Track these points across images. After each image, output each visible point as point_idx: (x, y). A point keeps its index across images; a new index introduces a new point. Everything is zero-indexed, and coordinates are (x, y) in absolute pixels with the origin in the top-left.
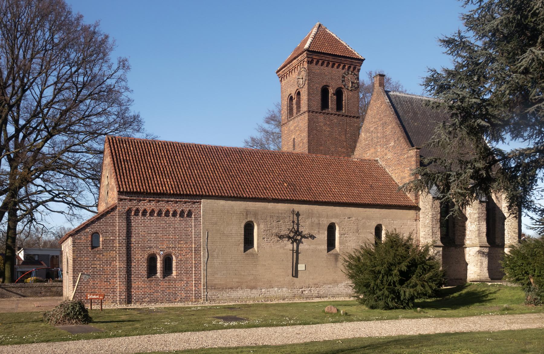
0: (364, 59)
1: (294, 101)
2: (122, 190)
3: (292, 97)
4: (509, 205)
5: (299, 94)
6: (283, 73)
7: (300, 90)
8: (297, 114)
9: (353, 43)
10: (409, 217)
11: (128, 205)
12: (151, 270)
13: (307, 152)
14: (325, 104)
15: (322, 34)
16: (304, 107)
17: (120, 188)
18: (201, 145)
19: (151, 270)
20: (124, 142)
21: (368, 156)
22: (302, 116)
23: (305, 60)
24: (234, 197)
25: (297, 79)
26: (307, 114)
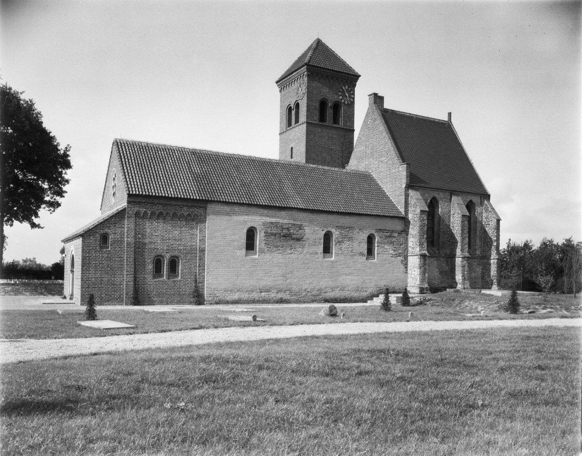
0: (360, 76)
1: (293, 112)
2: (131, 193)
3: (291, 107)
4: (559, 246)
5: (297, 106)
6: (283, 82)
7: (299, 102)
8: (295, 124)
9: (350, 54)
10: (472, 371)
11: (136, 209)
12: (158, 270)
13: (304, 161)
14: (322, 118)
15: (319, 47)
16: (303, 118)
17: (129, 191)
18: (184, 148)
19: (158, 270)
20: (164, 150)
21: (361, 168)
22: (300, 127)
23: (306, 73)
24: (232, 203)
25: (299, 91)
26: (305, 125)
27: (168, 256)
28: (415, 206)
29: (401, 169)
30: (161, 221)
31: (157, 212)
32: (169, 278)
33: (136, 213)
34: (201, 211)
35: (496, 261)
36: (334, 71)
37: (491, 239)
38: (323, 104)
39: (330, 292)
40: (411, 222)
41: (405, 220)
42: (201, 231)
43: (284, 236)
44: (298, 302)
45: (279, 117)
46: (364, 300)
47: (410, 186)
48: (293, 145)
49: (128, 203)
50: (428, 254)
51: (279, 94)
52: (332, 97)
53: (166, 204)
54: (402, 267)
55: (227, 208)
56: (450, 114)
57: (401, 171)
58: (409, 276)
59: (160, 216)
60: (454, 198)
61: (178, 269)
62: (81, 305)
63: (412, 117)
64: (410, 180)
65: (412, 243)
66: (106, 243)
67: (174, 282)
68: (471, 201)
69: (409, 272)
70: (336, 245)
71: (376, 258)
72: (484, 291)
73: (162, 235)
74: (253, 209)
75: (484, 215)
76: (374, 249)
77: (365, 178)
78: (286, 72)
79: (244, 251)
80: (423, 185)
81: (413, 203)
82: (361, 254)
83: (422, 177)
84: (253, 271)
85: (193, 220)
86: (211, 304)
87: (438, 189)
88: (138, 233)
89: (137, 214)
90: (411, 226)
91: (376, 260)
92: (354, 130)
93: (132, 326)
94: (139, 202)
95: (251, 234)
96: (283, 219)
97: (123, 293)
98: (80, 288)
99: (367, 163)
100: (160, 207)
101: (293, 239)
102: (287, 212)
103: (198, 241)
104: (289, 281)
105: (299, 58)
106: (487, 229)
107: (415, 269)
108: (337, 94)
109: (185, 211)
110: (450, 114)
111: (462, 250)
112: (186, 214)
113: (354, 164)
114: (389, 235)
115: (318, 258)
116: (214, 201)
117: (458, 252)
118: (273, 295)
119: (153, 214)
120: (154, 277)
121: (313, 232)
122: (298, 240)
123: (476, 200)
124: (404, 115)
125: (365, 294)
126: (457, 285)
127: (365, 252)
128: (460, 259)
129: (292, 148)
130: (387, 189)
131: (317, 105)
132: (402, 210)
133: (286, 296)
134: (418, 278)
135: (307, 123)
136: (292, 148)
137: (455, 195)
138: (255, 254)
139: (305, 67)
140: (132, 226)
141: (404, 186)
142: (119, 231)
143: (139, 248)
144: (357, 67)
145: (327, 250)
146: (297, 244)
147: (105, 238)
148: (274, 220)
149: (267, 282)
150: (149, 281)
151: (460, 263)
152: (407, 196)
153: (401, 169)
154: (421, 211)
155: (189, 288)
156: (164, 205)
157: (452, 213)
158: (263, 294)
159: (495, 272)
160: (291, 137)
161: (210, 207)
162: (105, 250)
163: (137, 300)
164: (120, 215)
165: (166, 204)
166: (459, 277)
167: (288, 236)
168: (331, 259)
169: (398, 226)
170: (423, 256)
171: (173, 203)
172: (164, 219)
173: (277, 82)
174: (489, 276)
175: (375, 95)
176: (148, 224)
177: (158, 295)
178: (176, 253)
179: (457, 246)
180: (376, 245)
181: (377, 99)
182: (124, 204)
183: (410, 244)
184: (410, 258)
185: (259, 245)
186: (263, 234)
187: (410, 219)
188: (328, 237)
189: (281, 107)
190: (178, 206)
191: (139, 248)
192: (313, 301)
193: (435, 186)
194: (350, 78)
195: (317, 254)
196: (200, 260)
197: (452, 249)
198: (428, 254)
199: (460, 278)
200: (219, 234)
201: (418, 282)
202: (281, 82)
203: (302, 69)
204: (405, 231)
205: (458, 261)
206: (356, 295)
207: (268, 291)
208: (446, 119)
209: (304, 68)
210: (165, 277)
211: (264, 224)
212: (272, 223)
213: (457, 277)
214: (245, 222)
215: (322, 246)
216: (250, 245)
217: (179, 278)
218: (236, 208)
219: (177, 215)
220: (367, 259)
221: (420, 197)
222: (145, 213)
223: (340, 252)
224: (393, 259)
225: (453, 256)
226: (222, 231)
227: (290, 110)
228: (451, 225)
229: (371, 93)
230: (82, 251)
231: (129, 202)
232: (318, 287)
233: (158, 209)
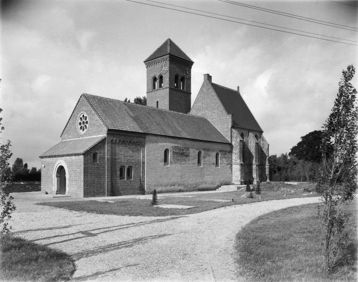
5: (161, 77)
7: (163, 75)
27: (127, 166)
28: (236, 137)
29: (227, 117)
30: (123, 145)
31: (122, 140)
32: (127, 180)
33: (111, 140)
34: (141, 139)
35: (268, 167)
36: (182, 59)
37: (265, 155)
38: (176, 77)
39: (201, 185)
40: (234, 146)
41: (230, 145)
42: (143, 151)
43: (181, 154)
44: (187, 191)
45: (146, 83)
46: (215, 189)
47: (233, 127)
48: (158, 100)
49: (107, 135)
50: (243, 164)
51: (146, 69)
52: (181, 74)
53: (126, 136)
54: (230, 171)
55: (155, 138)
56: (238, 87)
57: (228, 119)
58: (233, 175)
59: (124, 143)
60: (250, 133)
61: (132, 174)
62: (84, 197)
63: (224, 88)
64: (233, 124)
65: (234, 158)
66: (95, 159)
67: (130, 181)
68: (256, 135)
69: (233, 173)
70: (203, 159)
71: (219, 165)
72: (286, 183)
73: (124, 154)
74: (167, 139)
75: (262, 142)
76: (218, 161)
77: (204, 121)
78: (150, 57)
79: (163, 163)
80: (238, 126)
81: (235, 136)
82: (213, 164)
83: (236, 122)
84: (167, 174)
85: (139, 145)
86: (148, 194)
87: (243, 129)
88: (113, 154)
89: (112, 141)
90: (234, 149)
91: (169, 165)
92: (191, 93)
93: (193, 207)
94: (113, 134)
95: (166, 152)
96: (180, 144)
97: (105, 189)
98: (83, 187)
99: (203, 112)
100: (123, 137)
101: (185, 156)
102: (182, 140)
103: (141, 157)
104: (183, 179)
105: (158, 49)
106: (263, 150)
107: (237, 172)
108: (183, 72)
109: (135, 140)
110: (238, 87)
111: (256, 161)
112: (136, 141)
113: (193, 112)
114: (224, 152)
115: (195, 166)
116: (150, 134)
117: (254, 162)
118: (177, 188)
119: (120, 141)
120: (120, 179)
121: (193, 153)
122: (187, 156)
123: (258, 134)
124: (220, 87)
125: (215, 186)
126: (253, 180)
127: (215, 163)
128: (255, 166)
129: (157, 102)
130: (218, 127)
131: (174, 78)
132: (229, 140)
133: (182, 188)
134: (239, 176)
135: (170, 88)
136: (157, 102)
137: (251, 132)
138: (219, 166)
139: (168, 55)
140: (110, 148)
141: (230, 127)
142: (102, 151)
143: (113, 161)
144: (193, 59)
145: (199, 162)
146: (187, 159)
147: (95, 156)
148: (176, 145)
149: (174, 180)
150: (120, 182)
151: (255, 168)
152: (231, 132)
153: (227, 117)
154: (240, 140)
155: (137, 185)
156: (125, 136)
157: (249, 141)
158: (172, 187)
159: (268, 173)
160: (157, 95)
161: (148, 138)
162: (95, 163)
163: (113, 193)
164: (102, 142)
165: (126, 136)
166: (255, 175)
167: (182, 154)
168: (168, 166)
169: (228, 148)
170: (241, 164)
171: (130, 134)
172: (125, 144)
173: (145, 62)
174: (265, 174)
175: (208, 75)
176: (117, 147)
177: (122, 190)
178: (131, 165)
179: (253, 159)
180: (219, 159)
181: (209, 77)
182: (105, 135)
183: (234, 158)
184: (233, 166)
185: (170, 159)
186: (172, 153)
187: (233, 145)
188: (199, 154)
189: (148, 77)
190: (132, 136)
191: (113, 161)
192: (194, 190)
193: (243, 127)
194: (189, 63)
195: (195, 164)
196: (142, 168)
197: (250, 161)
198: (243, 164)
199: (255, 176)
200: (152, 153)
201: (239, 179)
202: (148, 62)
203: (166, 56)
204: (231, 152)
205: (254, 167)
206: (211, 186)
207: (174, 185)
208: (236, 90)
209: (167, 56)
210: (125, 179)
211: (172, 147)
212: (176, 147)
213: (253, 175)
214: (164, 146)
215: (197, 159)
216: (166, 160)
217: (133, 179)
218: (159, 138)
219: (131, 142)
220: (216, 166)
221: (238, 133)
222: (116, 141)
223: (205, 163)
224: (226, 166)
225: (251, 164)
226: (152, 152)
227: (155, 79)
228: (249, 148)
229: (206, 74)
230: (84, 164)
231: (108, 134)
232: (196, 183)
233: (122, 138)
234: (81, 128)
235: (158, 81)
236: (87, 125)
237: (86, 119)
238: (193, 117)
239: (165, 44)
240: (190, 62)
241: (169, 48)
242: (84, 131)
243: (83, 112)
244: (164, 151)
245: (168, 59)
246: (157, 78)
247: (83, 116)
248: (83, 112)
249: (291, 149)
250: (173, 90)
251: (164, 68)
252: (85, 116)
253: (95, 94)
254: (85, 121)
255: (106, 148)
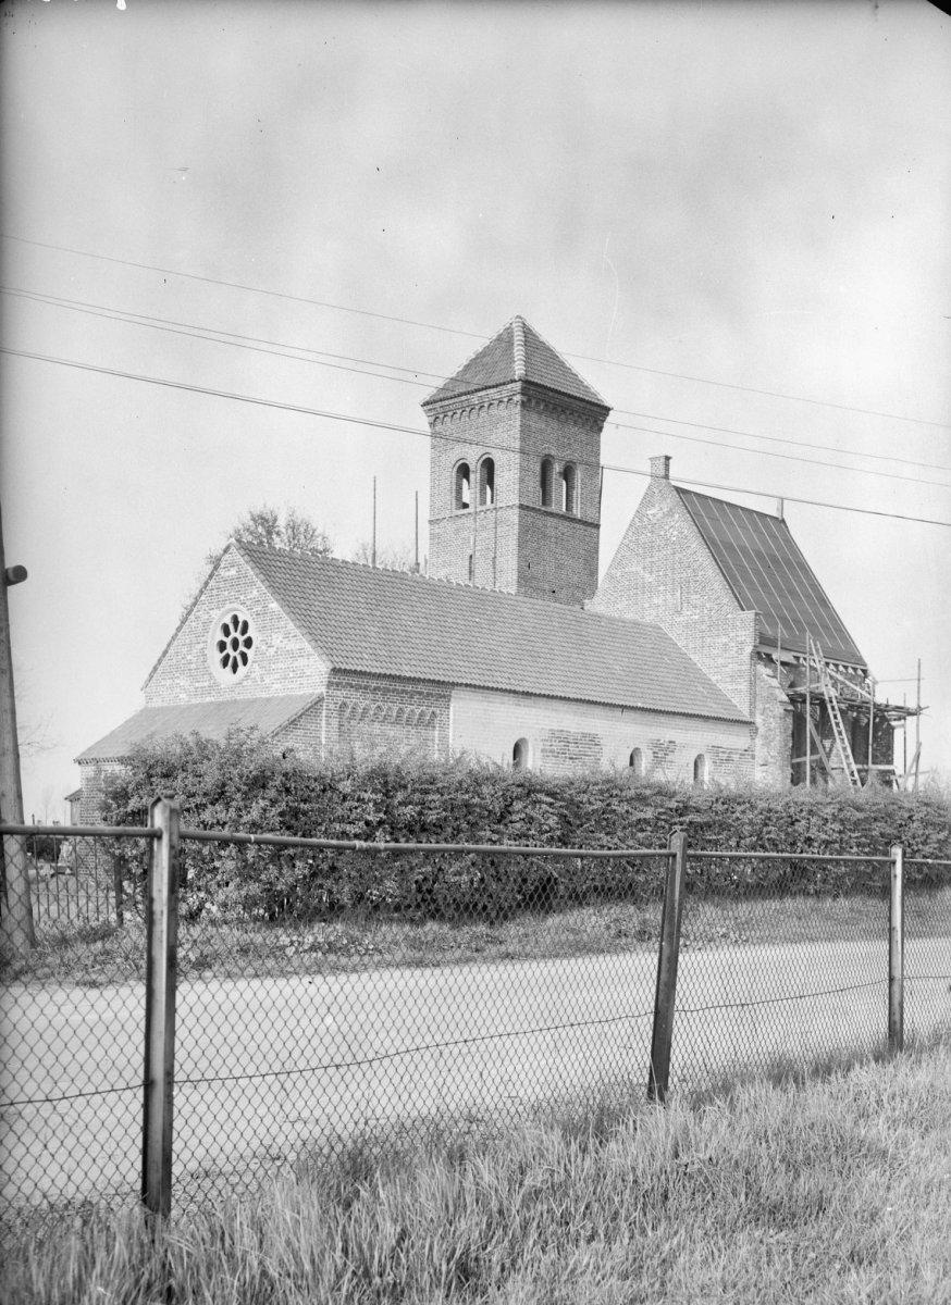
5: (489, 466)
57: (742, 630)
109: (414, 708)
113: (597, 605)
227: (464, 471)
234: (225, 662)
235: (475, 477)
236: (250, 653)
237: (244, 631)
238: (598, 617)
239: (504, 341)
240: (599, 406)
241: (518, 352)
242: (235, 672)
243: (235, 605)
244: (513, 746)
245: (518, 398)
246: (472, 468)
247: (235, 620)
248: (235, 605)
249: (20, 574)
250: (535, 512)
251: (503, 433)
252: (241, 620)
253: (601, 536)
254: (241, 639)
255: (323, 733)
